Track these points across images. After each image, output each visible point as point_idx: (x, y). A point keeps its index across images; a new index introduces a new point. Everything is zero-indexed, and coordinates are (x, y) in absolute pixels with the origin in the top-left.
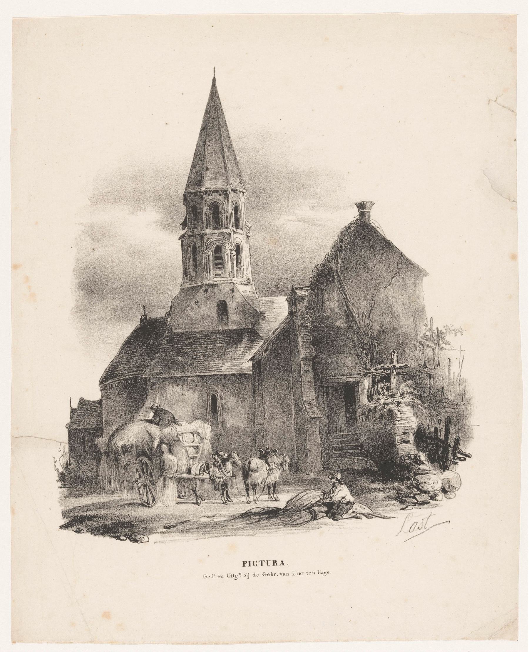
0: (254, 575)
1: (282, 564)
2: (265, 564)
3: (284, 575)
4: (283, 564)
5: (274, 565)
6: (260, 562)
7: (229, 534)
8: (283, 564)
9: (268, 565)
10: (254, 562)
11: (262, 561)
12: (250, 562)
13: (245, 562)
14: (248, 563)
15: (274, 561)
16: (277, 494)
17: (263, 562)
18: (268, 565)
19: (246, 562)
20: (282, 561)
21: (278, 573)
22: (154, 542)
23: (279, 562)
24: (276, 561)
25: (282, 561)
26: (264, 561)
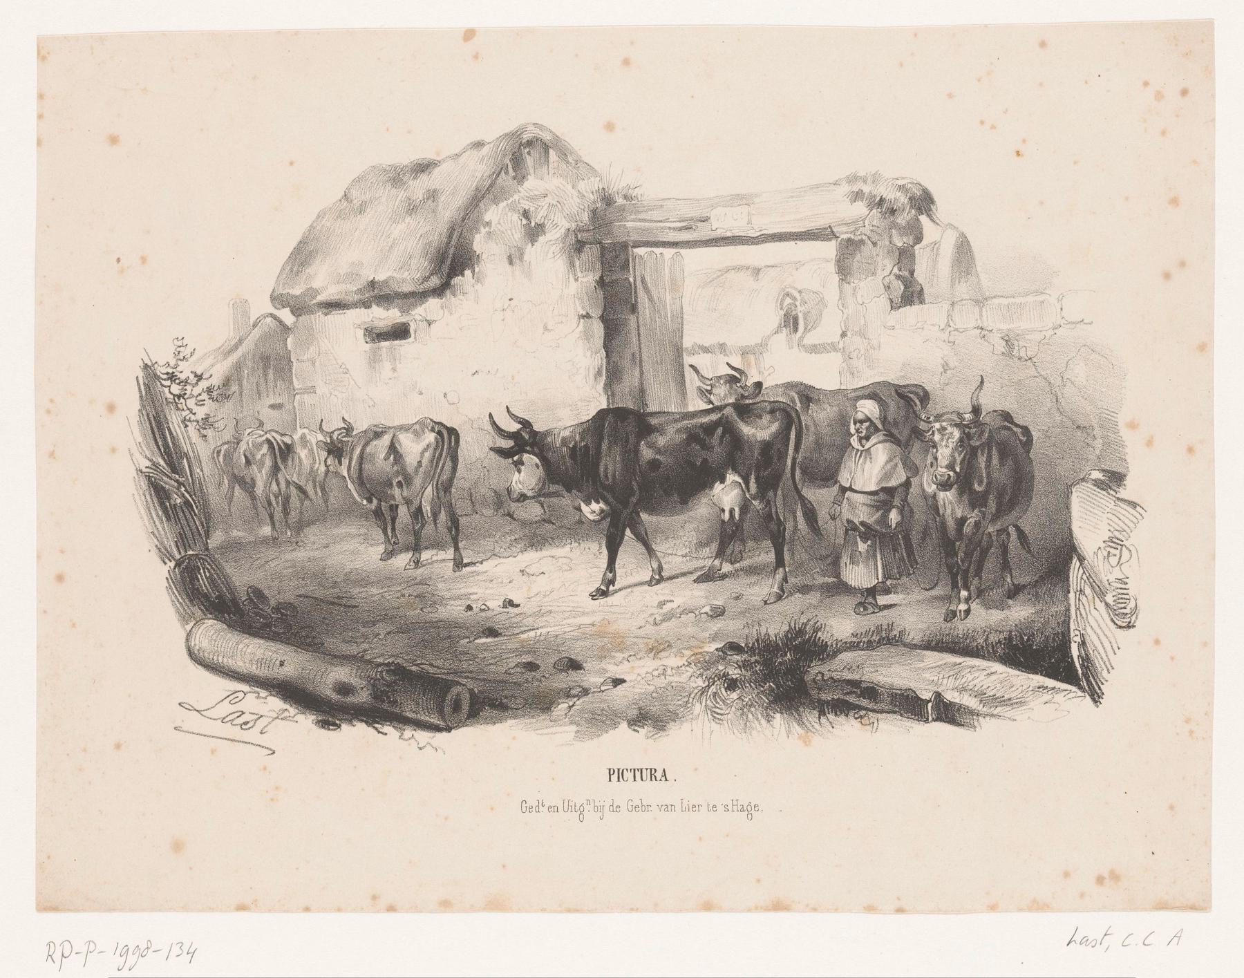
6: (632, 770)
9: (642, 780)
11: (634, 770)
24: (655, 770)
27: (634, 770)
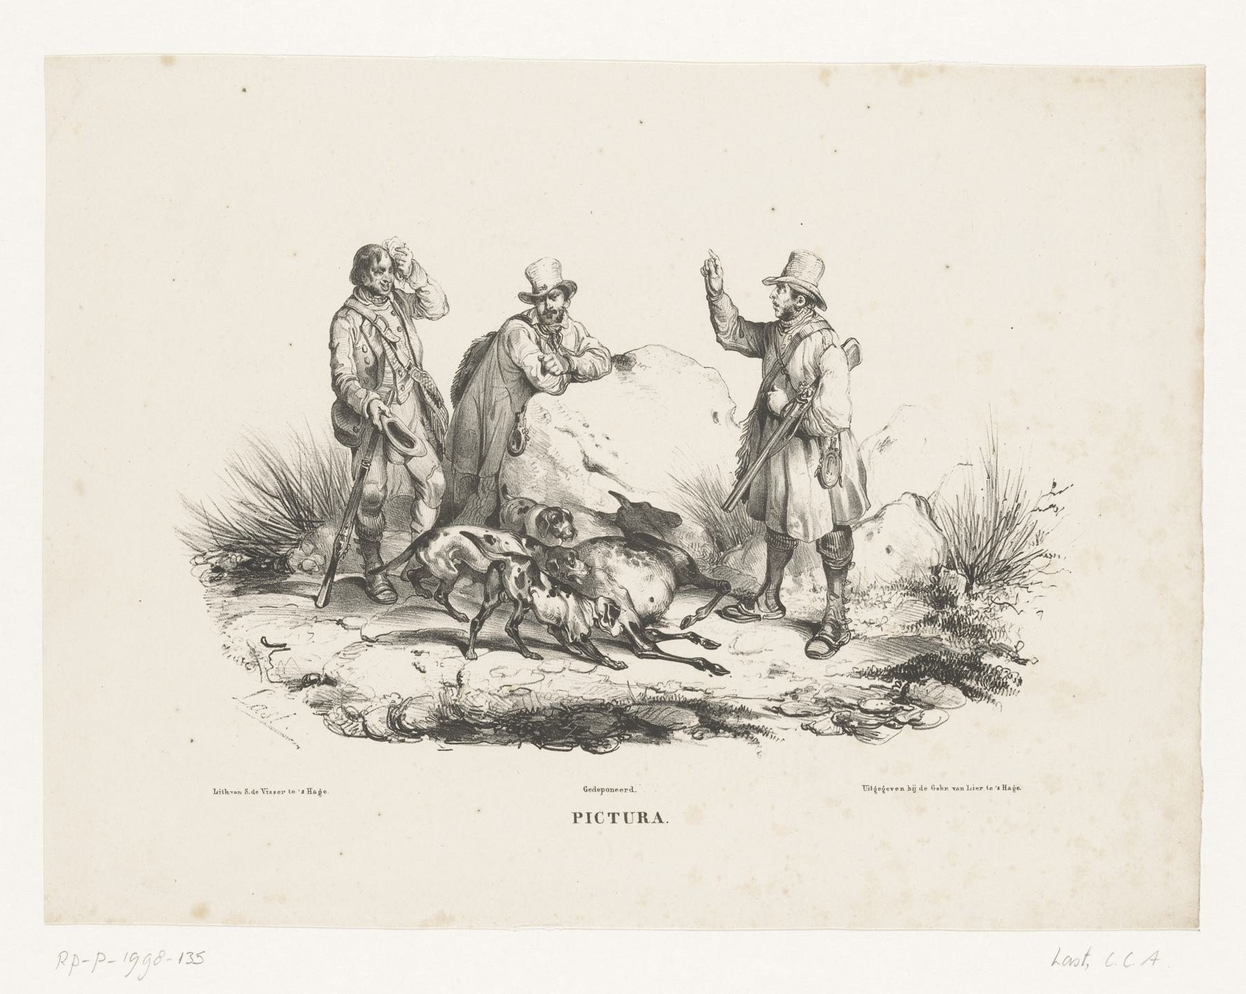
0: (921, 789)
1: (657, 821)
2: (619, 819)
3: (236, 793)
4: (661, 821)
5: (640, 822)
6: (611, 815)
7: (758, 929)
8: (661, 821)
9: (626, 822)
10: (597, 815)
11: (613, 814)
12: (588, 814)
13: (578, 815)
14: (585, 816)
15: (640, 814)
16: (614, 368)
17: (616, 815)
18: (626, 822)
19: (581, 815)
20: (658, 814)
21: (298, 794)
22: (1134, 952)
23: (651, 817)
24: (645, 814)
25: (658, 814)
26: (618, 814)
27: (613, 814)
